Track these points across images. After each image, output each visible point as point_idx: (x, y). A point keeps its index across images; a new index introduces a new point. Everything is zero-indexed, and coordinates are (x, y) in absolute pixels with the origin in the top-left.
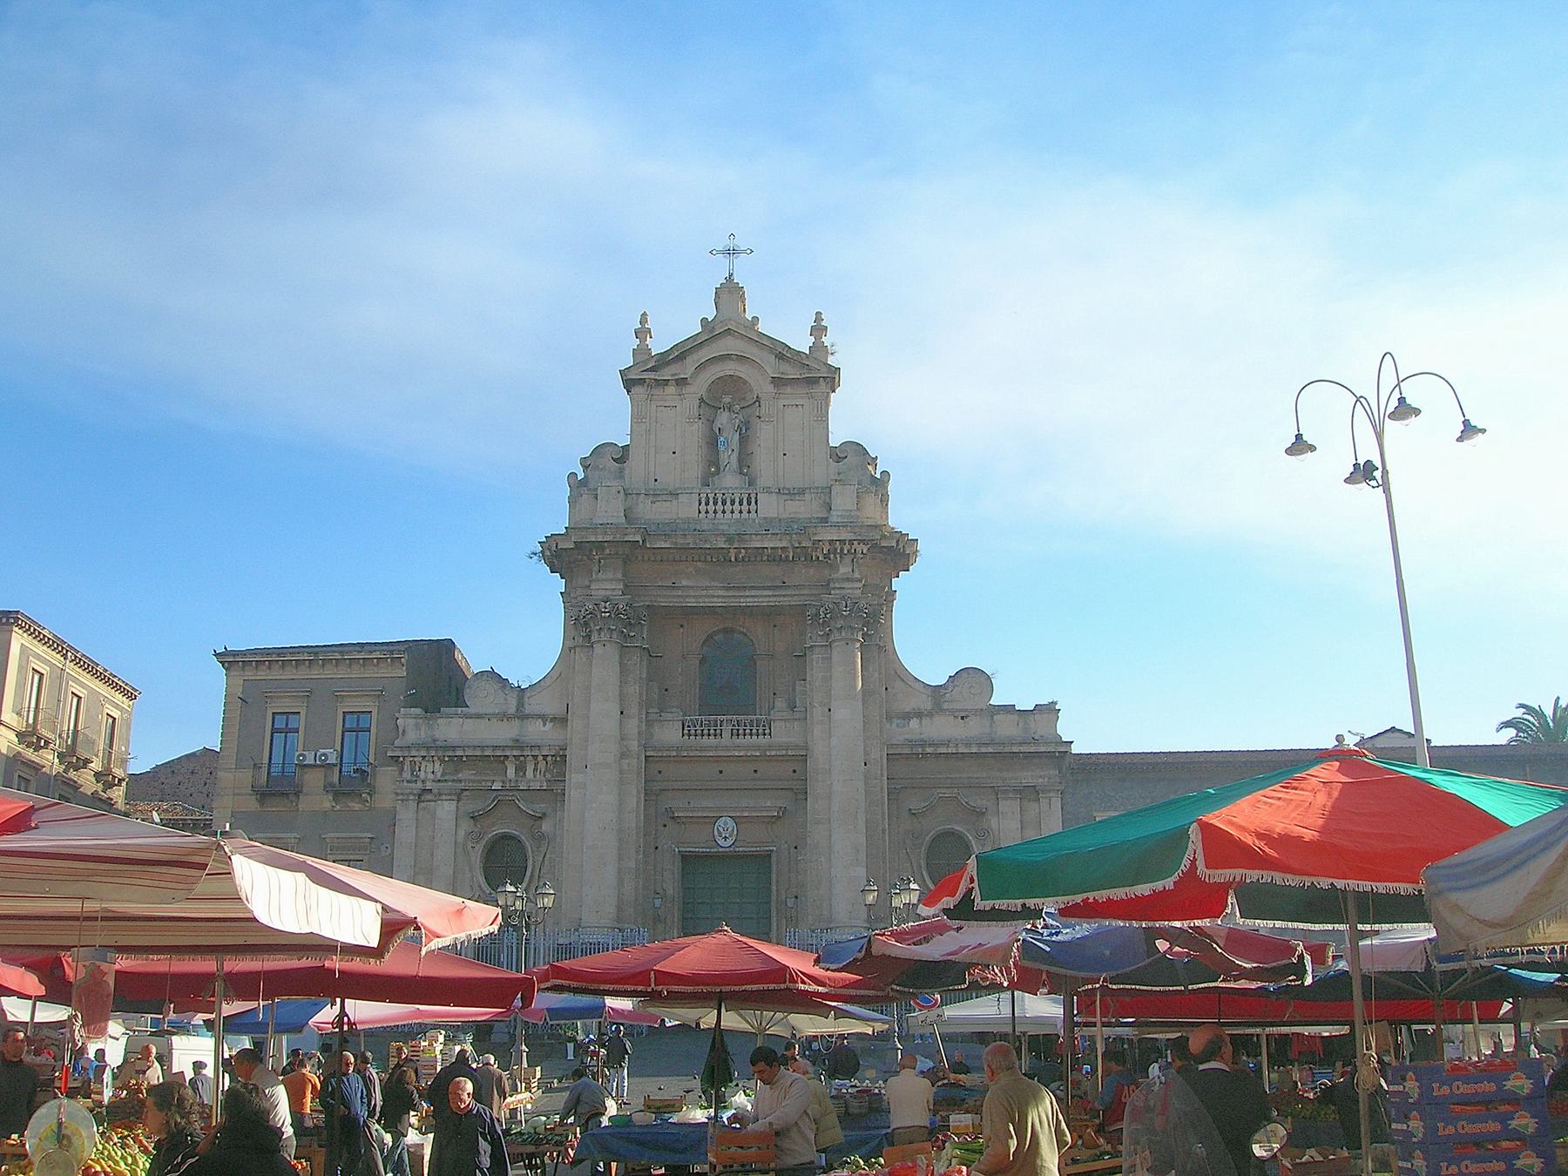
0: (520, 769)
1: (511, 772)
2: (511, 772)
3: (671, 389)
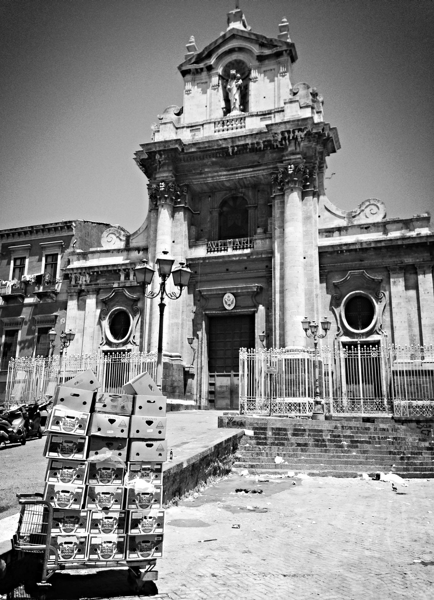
0: (127, 276)
1: (122, 278)
2: (122, 278)
3: (204, 74)
